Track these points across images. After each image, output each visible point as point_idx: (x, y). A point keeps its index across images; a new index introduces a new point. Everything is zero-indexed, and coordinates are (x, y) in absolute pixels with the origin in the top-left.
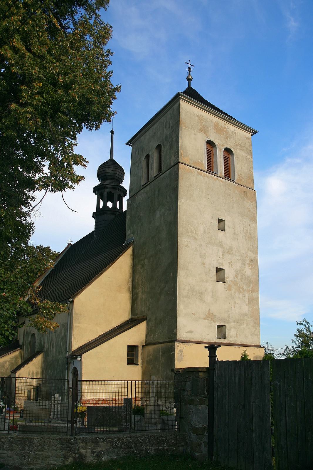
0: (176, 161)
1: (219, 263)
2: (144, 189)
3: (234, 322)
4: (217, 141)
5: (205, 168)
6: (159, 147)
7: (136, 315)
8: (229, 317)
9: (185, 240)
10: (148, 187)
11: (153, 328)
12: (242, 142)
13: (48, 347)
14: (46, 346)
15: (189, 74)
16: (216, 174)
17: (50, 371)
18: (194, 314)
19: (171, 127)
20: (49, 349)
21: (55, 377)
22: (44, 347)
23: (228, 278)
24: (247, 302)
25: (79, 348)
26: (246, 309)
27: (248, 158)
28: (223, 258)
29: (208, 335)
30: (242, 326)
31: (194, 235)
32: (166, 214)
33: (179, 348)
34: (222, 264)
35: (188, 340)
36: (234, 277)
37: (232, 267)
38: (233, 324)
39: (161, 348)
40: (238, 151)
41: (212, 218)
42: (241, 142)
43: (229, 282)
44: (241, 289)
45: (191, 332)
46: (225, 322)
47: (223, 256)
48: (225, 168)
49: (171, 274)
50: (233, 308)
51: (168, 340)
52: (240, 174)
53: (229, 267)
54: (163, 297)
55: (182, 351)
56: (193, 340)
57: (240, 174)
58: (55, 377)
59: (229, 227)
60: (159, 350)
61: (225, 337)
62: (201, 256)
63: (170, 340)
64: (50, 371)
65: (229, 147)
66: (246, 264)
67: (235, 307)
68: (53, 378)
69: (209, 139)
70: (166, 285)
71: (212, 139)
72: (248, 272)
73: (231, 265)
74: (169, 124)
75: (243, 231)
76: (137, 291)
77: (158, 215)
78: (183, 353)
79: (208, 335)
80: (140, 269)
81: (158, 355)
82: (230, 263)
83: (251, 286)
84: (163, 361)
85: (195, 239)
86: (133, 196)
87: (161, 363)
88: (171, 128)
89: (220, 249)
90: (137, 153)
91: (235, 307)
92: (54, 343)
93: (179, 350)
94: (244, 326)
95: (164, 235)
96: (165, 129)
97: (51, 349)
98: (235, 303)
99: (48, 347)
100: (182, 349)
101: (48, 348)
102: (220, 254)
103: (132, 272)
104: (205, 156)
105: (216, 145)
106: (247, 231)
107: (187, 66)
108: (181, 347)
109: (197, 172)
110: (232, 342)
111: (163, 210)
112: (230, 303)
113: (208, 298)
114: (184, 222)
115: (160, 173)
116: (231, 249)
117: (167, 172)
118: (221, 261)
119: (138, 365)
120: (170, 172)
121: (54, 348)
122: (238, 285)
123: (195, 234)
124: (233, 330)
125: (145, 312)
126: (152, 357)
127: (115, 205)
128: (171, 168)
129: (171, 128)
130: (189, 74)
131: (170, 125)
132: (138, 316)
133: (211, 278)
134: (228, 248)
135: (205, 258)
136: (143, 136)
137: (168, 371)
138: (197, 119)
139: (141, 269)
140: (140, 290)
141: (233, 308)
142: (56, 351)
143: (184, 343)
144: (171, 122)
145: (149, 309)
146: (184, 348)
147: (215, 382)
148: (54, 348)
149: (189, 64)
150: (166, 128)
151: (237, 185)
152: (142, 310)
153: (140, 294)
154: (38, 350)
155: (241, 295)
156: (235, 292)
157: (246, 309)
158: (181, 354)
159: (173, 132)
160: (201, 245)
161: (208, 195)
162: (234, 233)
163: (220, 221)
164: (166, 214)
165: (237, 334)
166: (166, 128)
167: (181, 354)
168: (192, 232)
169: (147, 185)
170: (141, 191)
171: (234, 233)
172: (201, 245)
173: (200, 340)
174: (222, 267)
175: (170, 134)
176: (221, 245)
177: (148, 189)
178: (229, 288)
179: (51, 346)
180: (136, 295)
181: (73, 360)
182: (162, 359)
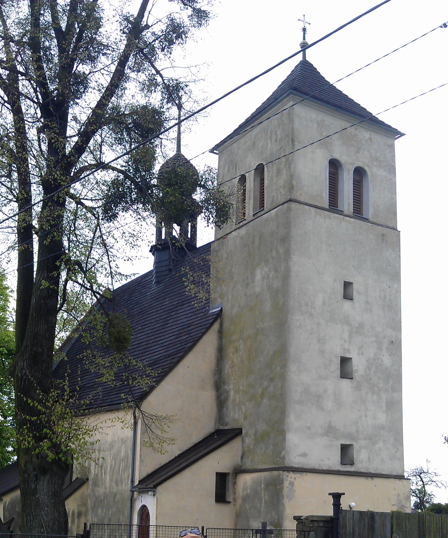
0: (285, 197)
1: (345, 350)
2: (238, 230)
3: (365, 439)
4: (344, 157)
5: (326, 204)
6: (260, 170)
7: (226, 426)
8: (357, 431)
9: (298, 318)
10: (244, 228)
11: (252, 446)
12: (381, 154)
13: (96, 472)
14: (93, 471)
15: (304, 38)
16: (341, 213)
17: (100, 511)
18: (309, 428)
19: (278, 139)
20: (99, 475)
21: (110, 520)
22: (90, 472)
23: (357, 371)
24: (384, 408)
25: (147, 476)
26: (382, 418)
27: (389, 179)
28: (350, 342)
29: (328, 458)
30: (377, 446)
31: (310, 310)
32: (271, 276)
33: (289, 479)
34: (349, 351)
35: (300, 467)
36: (365, 370)
37: (362, 354)
38: (363, 443)
39: (263, 478)
40: (375, 169)
41: (335, 281)
42: (378, 155)
43: (357, 378)
44: (376, 388)
45: (304, 455)
46: (353, 439)
47: (349, 338)
48: (355, 193)
49: (278, 368)
50: (364, 418)
51: (273, 466)
52: (377, 206)
53: (359, 354)
54: (265, 401)
55: (292, 484)
56: (307, 467)
57: (377, 206)
58: (110, 520)
59: (359, 293)
60: (261, 481)
61: (352, 464)
62: (319, 340)
63: (276, 466)
64: (100, 511)
65: (360, 165)
66: (384, 348)
67: (366, 416)
68: (106, 522)
69: (332, 156)
70: (271, 384)
71: (336, 156)
72: (387, 360)
73: (360, 352)
74: (276, 134)
75: (380, 297)
76: (228, 388)
77: (258, 276)
78: (294, 488)
79: (328, 458)
80: (231, 354)
81: (259, 488)
82: (361, 348)
83: (391, 383)
84: (267, 497)
85: (311, 315)
86: (221, 238)
87: (263, 500)
88: (278, 142)
89: (346, 327)
90: (226, 168)
91: (366, 416)
92: (107, 467)
93: (288, 482)
94: (380, 445)
95: (268, 308)
96: (269, 142)
97: (102, 475)
98: (367, 409)
99: (96, 472)
100: (292, 480)
101: (97, 475)
102: (346, 335)
103: (290, 465)
104: (327, 185)
105: (343, 164)
106: (385, 297)
107: (301, 25)
108: (291, 478)
109: (315, 212)
110: (363, 471)
111: (266, 269)
112: (359, 411)
113: (328, 404)
114: (296, 291)
115: (263, 210)
116: (361, 325)
117: (272, 211)
118: (346, 346)
119: (296, 518)
120: (277, 212)
121: (108, 475)
122: (372, 382)
123: (311, 307)
124: (363, 451)
125: (240, 421)
126: (250, 491)
127: (183, 231)
128: (279, 208)
129: (278, 142)
130: (304, 38)
131: (277, 137)
132: (228, 426)
133: (333, 372)
134: (357, 326)
135: (324, 344)
136: (235, 143)
137: (273, 513)
138: (316, 127)
139: (233, 355)
140: (231, 387)
141: (364, 418)
142: (111, 480)
143: (295, 472)
144: (278, 133)
145: (245, 418)
146: (295, 478)
147: (340, 532)
148: (108, 475)
149: (303, 21)
150: (271, 140)
151: (372, 225)
152: (235, 417)
153: (232, 393)
154: (79, 476)
155: (375, 397)
156: (367, 393)
157: (382, 418)
158: (291, 488)
159: (282, 150)
160: (320, 324)
161: (330, 246)
162: (367, 302)
163: (347, 285)
164: (271, 276)
165: (369, 458)
166: (271, 140)
167: (291, 488)
168: (307, 305)
169: (243, 226)
170: (233, 233)
171: (367, 302)
172: (318, 324)
173: (317, 467)
174: (348, 356)
175: (277, 151)
176: (346, 321)
177: (244, 232)
178: (358, 388)
179: (103, 471)
180: (225, 395)
181: (141, 495)
182: (264, 494)
